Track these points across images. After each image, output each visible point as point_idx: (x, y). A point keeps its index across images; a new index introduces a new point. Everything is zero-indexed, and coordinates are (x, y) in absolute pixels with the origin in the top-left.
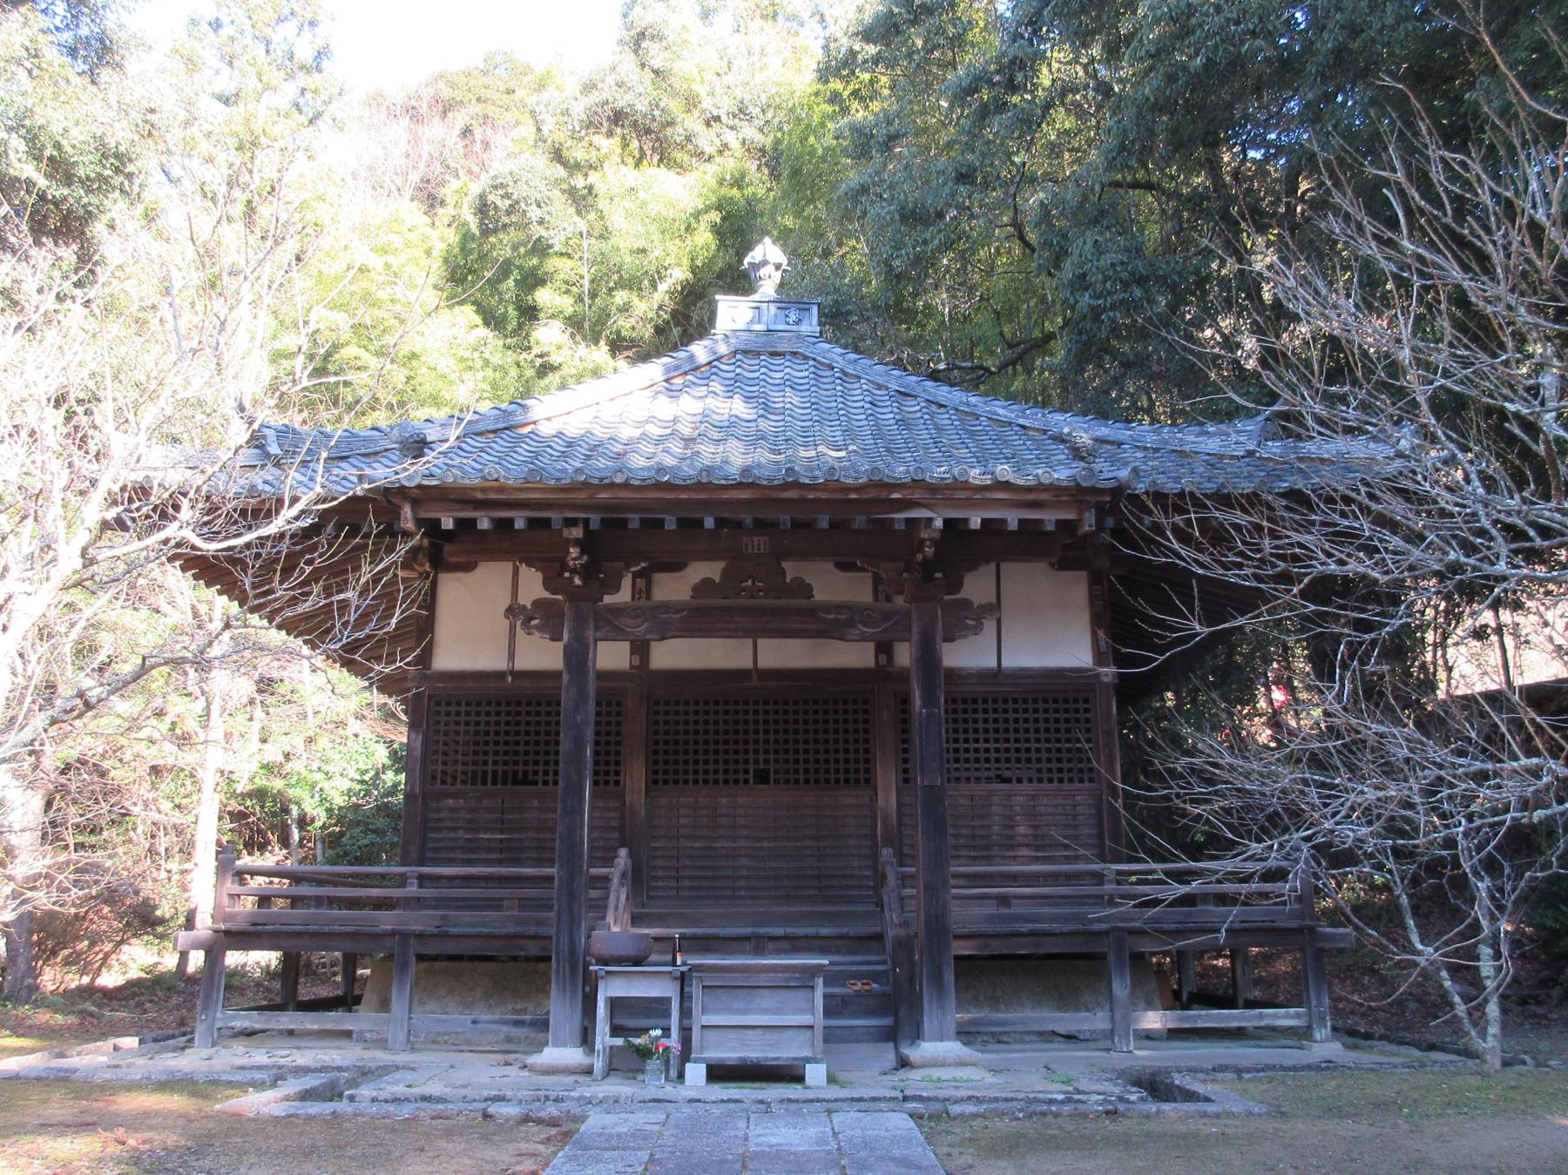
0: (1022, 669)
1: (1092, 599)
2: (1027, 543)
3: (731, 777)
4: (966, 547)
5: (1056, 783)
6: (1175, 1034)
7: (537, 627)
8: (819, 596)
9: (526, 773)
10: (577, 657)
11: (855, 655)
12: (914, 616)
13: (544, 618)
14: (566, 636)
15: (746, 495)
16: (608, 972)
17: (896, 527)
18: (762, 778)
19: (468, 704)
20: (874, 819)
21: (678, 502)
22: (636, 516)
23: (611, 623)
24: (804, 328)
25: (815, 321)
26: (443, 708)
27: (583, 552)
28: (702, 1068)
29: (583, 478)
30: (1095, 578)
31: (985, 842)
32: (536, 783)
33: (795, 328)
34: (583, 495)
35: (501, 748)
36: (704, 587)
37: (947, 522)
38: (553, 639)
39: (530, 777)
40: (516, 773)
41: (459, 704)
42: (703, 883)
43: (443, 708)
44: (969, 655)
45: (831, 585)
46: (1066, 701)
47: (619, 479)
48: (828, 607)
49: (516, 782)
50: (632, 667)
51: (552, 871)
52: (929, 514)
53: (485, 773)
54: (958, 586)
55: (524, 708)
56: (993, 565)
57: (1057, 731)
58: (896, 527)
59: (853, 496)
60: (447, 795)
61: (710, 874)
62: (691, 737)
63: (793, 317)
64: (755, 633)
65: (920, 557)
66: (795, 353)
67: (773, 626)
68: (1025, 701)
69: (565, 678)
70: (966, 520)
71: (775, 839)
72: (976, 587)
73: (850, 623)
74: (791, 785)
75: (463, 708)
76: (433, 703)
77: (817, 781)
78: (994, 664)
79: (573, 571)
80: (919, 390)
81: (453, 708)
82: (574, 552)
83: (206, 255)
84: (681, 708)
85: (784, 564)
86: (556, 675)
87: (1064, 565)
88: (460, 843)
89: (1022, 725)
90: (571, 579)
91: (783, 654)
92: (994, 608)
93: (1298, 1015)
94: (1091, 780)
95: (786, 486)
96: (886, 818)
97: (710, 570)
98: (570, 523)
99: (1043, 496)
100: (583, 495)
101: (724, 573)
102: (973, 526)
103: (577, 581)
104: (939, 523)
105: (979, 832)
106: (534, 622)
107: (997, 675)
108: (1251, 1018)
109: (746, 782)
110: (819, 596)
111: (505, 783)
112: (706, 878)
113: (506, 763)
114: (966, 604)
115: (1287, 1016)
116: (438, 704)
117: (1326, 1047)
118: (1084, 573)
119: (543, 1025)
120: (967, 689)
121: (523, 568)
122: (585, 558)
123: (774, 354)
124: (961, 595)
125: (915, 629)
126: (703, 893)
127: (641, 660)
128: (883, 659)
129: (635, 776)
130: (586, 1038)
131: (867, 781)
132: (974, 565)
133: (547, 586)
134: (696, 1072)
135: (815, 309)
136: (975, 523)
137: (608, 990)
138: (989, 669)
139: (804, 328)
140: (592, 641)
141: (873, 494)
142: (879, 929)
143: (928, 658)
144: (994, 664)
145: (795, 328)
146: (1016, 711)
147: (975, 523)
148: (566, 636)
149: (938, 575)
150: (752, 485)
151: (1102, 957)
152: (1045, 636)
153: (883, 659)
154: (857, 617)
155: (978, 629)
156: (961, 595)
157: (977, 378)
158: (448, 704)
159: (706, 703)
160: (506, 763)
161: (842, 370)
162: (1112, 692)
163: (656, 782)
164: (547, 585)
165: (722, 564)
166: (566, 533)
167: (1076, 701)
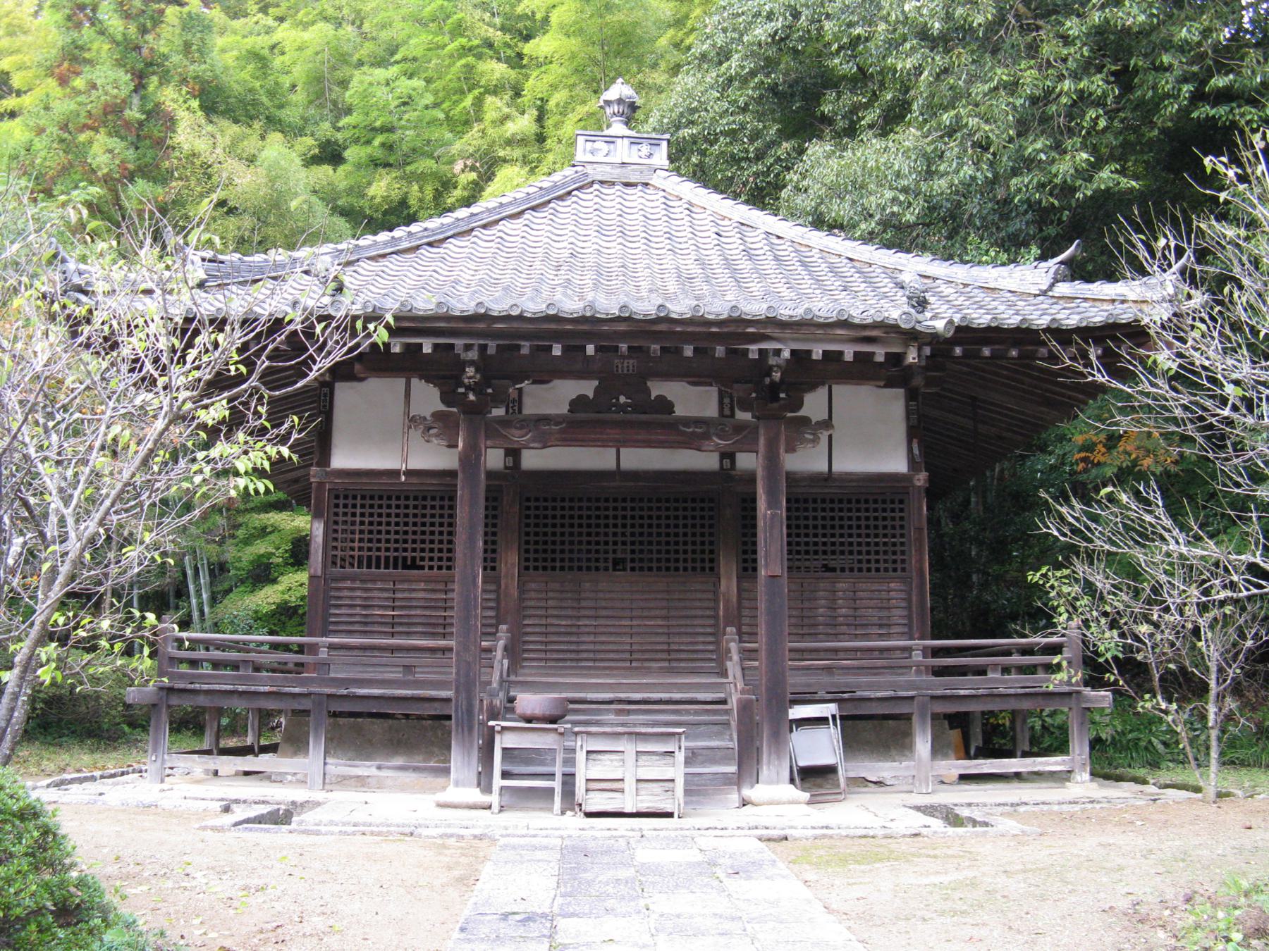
0: (847, 474)
2: (861, 370)
3: (593, 564)
4: (808, 372)
5: (856, 572)
6: (964, 778)
7: (437, 436)
8: (679, 411)
9: (414, 559)
10: (471, 459)
11: (704, 460)
12: (762, 431)
13: (442, 425)
14: (461, 444)
15: (622, 327)
16: (504, 728)
17: (751, 356)
18: (618, 564)
19: (363, 498)
20: (716, 600)
21: (568, 332)
22: (527, 344)
23: (494, 431)
26: (341, 502)
27: (477, 371)
29: (483, 311)
30: (912, 395)
31: (812, 621)
32: (422, 568)
34: (482, 325)
35: (392, 537)
36: (578, 403)
37: (793, 352)
38: (449, 446)
40: (405, 559)
41: (355, 497)
42: (568, 656)
43: (341, 502)
44: (807, 460)
45: (693, 401)
46: (884, 502)
47: (515, 312)
48: (687, 421)
49: (405, 567)
50: (506, 468)
51: (452, 643)
52: (778, 346)
53: (378, 558)
54: (800, 405)
56: (827, 387)
57: (876, 527)
58: (751, 356)
59: (714, 330)
60: (343, 579)
61: (573, 647)
62: (681, 530)
64: (619, 444)
65: (767, 380)
66: (647, 184)
67: (640, 437)
68: (849, 501)
69: (460, 476)
70: (809, 352)
71: (631, 618)
72: (813, 405)
73: (706, 436)
74: (715, 565)
75: (359, 502)
76: (332, 497)
77: (694, 569)
78: (825, 468)
79: (468, 388)
81: (350, 502)
82: (470, 371)
84: (566, 504)
85: (649, 384)
86: (452, 474)
87: (889, 384)
88: (357, 619)
90: (465, 395)
91: (640, 459)
92: (827, 424)
93: (1064, 762)
95: (658, 320)
96: (727, 601)
97: (588, 388)
98: (468, 347)
99: (874, 333)
100: (482, 325)
101: (597, 391)
102: (814, 357)
103: (472, 397)
104: (786, 354)
105: (806, 613)
106: (432, 431)
107: (829, 477)
109: (606, 569)
110: (679, 411)
112: (571, 651)
113: (396, 550)
114: (805, 421)
115: (1057, 763)
116: (337, 497)
117: (1083, 786)
118: (901, 391)
119: (447, 771)
120: (799, 490)
121: (415, 382)
122: (478, 376)
123: (627, 185)
124: (801, 413)
125: (762, 441)
126: (568, 664)
127: (514, 462)
128: (727, 463)
129: (510, 561)
130: (484, 782)
131: (712, 569)
132: (813, 387)
133: (443, 400)
135: (664, 144)
136: (817, 354)
137: (500, 743)
138: (822, 473)
140: (483, 447)
141: (731, 329)
142: (722, 695)
143: (772, 462)
144: (825, 468)
147: (817, 354)
148: (461, 444)
149: (783, 395)
150: (629, 319)
151: (907, 718)
152: (868, 441)
153: (727, 463)
154: (712, 431)
155: (815, 441)
156: (801, 413)
158: (346, 497)
159: (571, 500)
160: (396, 550)
161: (690, 203)
162: (923, 495)
163: (527, 568)
164: (445, 399)
165: (596, 383)
166: (463, 356)
167: (893, 502)
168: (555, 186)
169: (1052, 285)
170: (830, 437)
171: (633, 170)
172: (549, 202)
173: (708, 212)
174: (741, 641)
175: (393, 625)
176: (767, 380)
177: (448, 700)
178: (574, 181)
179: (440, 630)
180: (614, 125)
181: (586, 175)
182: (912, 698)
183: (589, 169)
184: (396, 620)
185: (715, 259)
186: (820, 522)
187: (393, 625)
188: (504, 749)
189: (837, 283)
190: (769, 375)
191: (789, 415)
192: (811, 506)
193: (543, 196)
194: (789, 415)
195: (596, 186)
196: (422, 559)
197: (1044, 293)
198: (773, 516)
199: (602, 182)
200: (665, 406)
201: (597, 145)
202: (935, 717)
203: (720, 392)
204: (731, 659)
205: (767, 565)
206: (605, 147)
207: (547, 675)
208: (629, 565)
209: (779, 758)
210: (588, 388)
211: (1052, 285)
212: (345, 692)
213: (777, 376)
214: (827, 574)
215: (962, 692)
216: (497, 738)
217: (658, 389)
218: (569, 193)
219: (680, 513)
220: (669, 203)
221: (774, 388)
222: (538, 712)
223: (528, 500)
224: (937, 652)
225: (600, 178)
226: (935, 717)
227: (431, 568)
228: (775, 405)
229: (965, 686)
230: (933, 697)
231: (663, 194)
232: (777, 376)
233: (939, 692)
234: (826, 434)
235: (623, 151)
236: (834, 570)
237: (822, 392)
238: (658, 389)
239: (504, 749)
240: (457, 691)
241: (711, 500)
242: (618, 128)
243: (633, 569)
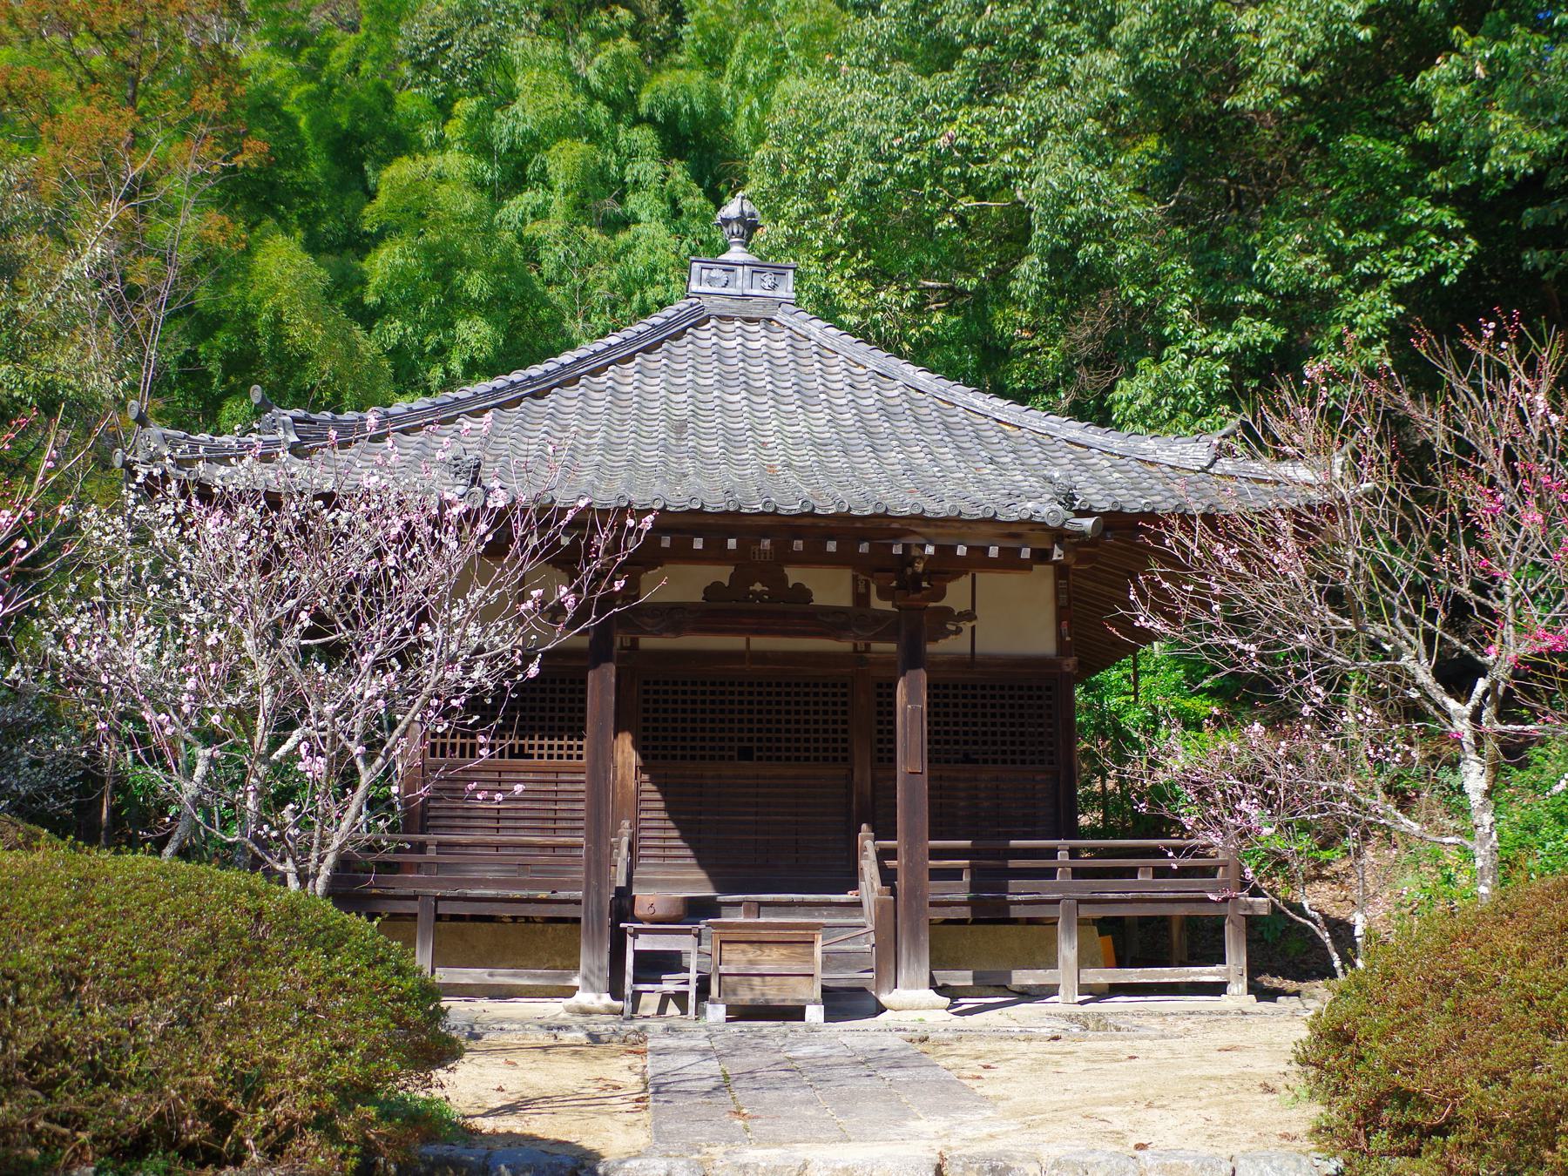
1: (1057, 592)
15: (766, 521)
24: (781, 293)
25: (790, 287)
28: (722, 1009)
32: (531, 756)
33: (770, 293)
36: (712, 591)
39: (526, 751)
41: (553, 681)
49: (512, 755)
53: (443, 745)
54: (941, 594)
55: (709, 688)
63: (769, 281)
71: (756, 814)
72: (956, 595)
78: (968, 649)
80: (897, 372)
83: (54, 156)
89: (989, 710)
92: (970, 615)
94: (1051, 763)
97: (722, 574)
108: (1195, 974)
111: (443, 755)
115: (1211, 974)
123: (748, 320)
132: (956, 575)
134: (716, 1012)
139: (781, 293)
145: (770, 293)
146: (562, 691)
157: (888, 344)
161: (819, 345)
165: (731, 569)
168: (668, 324)
169: (1214, 461)
170: (973, 628)
171: (756, 304)
172: (662, 341)
173: (841, 358)
174: (876, 839)
175: (498, 819)
176: (909, 571)
177: (578, 902)
178: (690, 316)
179: (550, 825)
180: (734, 248)
181: (702, 308)
182: (1057, 902)
183: (705, 302)
184: (502, 814)
185: (848, 418)
186: (960, 710)
187: (498, 819)
188: (636, 952)
189: (983, 454)
190: (911, 565)
191: (932, 604)
192: (951, 692)
193: (653, 335)
194: (932, 604)
195: (713, 322)
196: (531, 747)
197: (1204, 470)
198: (913, 710)
199: (720, 318)
200: (802, 594)
201: (714, 274)
202: (1082, 922)
203: (855, 579)
204: (867, 857)
205: (905, 762)
206: (723, 276)
207: (667, 873)
208: (756, 754)
209: (919, 966)
210: (722, 574)
211: (1214, 461)
212: (455, 893)
213: (920, 567)
214: (968, 766)
215: (1110, 896)
216: (629, 939)
217: (794, 575)
218: (684, 330)
219: (812, 699)
220: (797, 345)
221: (917, 578)
222: (660, 912)
223: (647, 683)
224: (936, 854)
225: (718, 312)
226: (1082, 922)
227: (541, 756)
228: (918, 596)
229: (1112, 889)
230: (1080, 901)
231: (787, 332)
232: (920, 567)
233: (1086, 896)
234: (970, 625)
235: (741, 282)
236: (976, 761)
237: (965, 581)
238: (794, 575)
239: (636, 952)
240: (587, 893)
241: (844, 686)
242: (736, 253)
243: (760, 758)
